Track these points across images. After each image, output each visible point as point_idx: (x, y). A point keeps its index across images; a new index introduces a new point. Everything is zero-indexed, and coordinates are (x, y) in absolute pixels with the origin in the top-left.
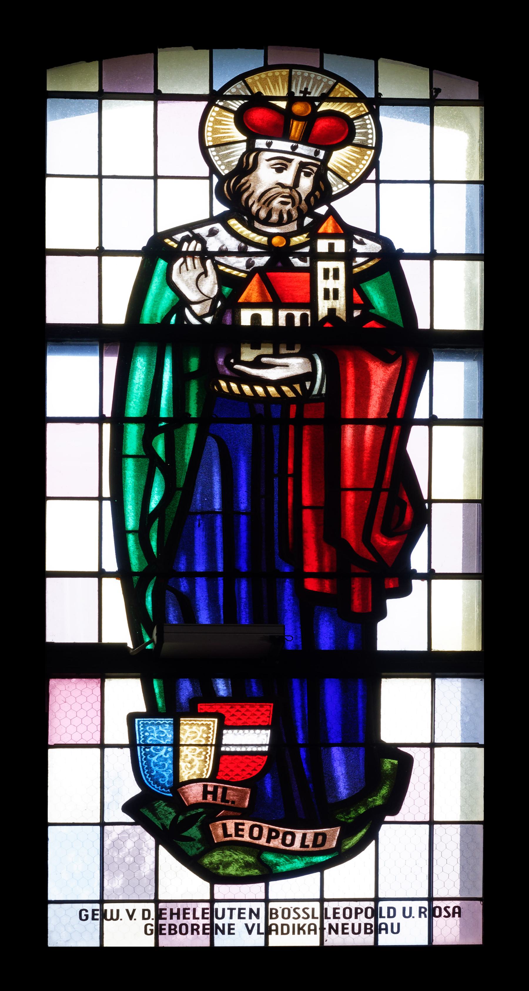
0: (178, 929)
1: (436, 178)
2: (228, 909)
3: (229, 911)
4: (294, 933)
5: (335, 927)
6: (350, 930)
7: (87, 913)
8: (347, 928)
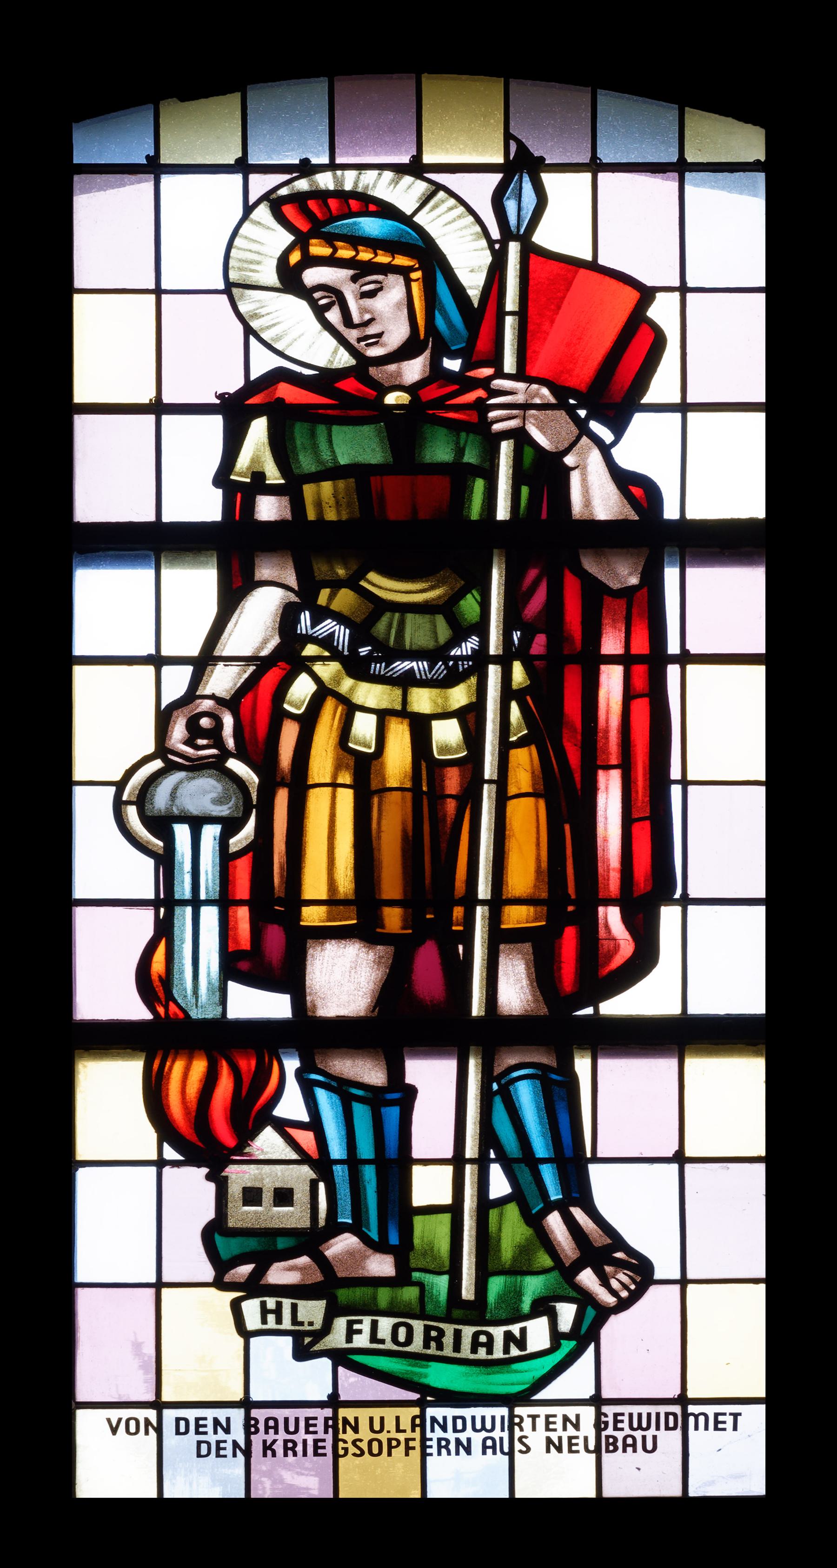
1: (164, 286)
2: (529, 1416)
3: (732, 1417)
4: (706, 1428)
6: (581, 1447)
7: (345, 1446)
8: (577, 1444)
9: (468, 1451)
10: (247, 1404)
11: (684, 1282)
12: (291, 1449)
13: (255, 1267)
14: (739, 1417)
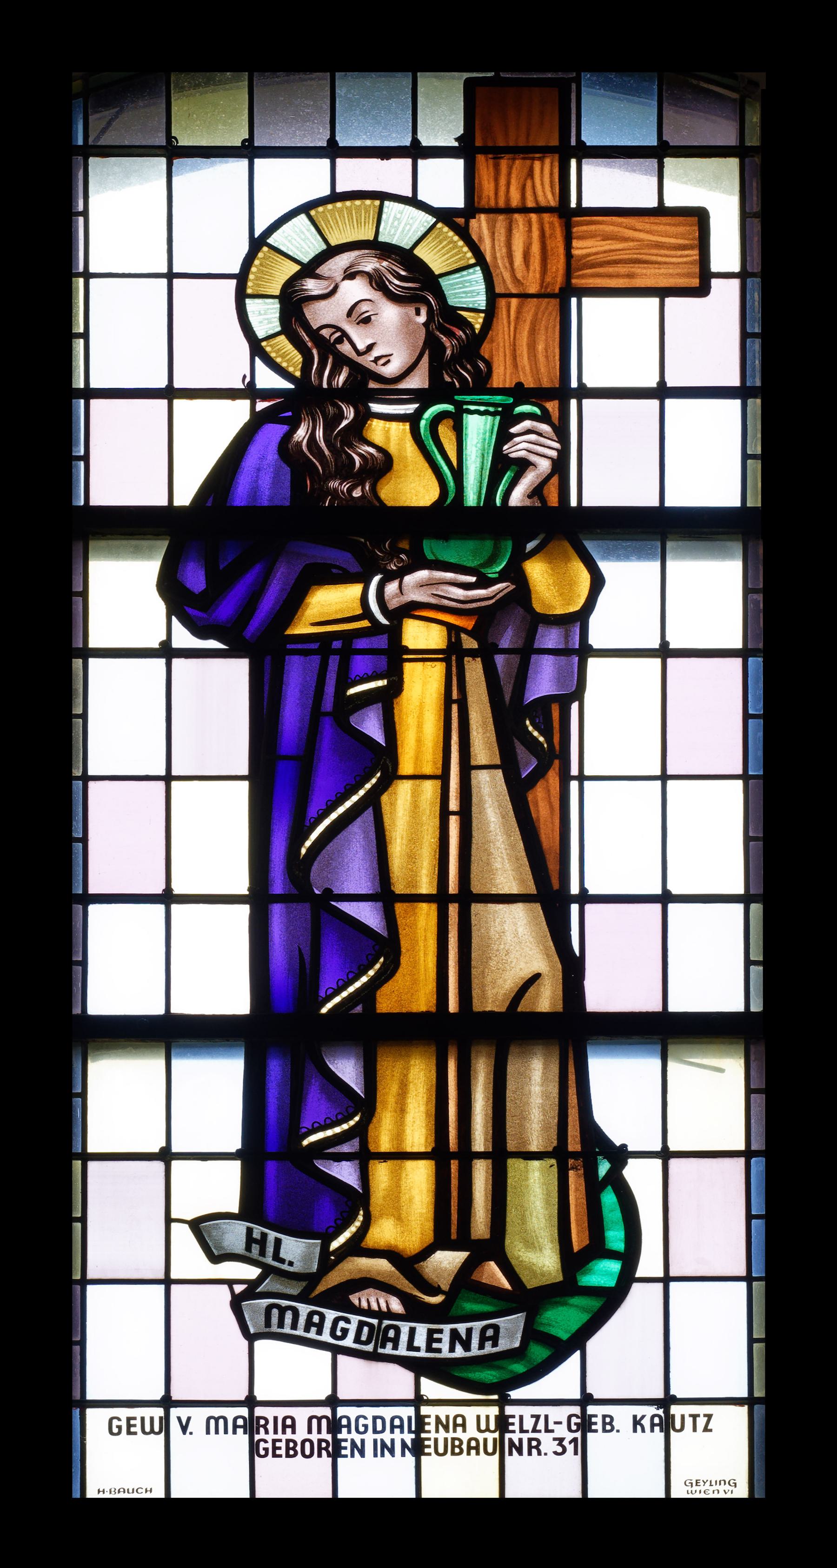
0: (298, 1448)
2: (690, 1416)
3: (691, 1419)
4: (226, 1432)
5: (517, 1443)
6: (138, 1429)
9: (362, 1453)
11: (666, 1280)
12: (535, 1447)
13: (469, 1256)
14: (698, 1419)
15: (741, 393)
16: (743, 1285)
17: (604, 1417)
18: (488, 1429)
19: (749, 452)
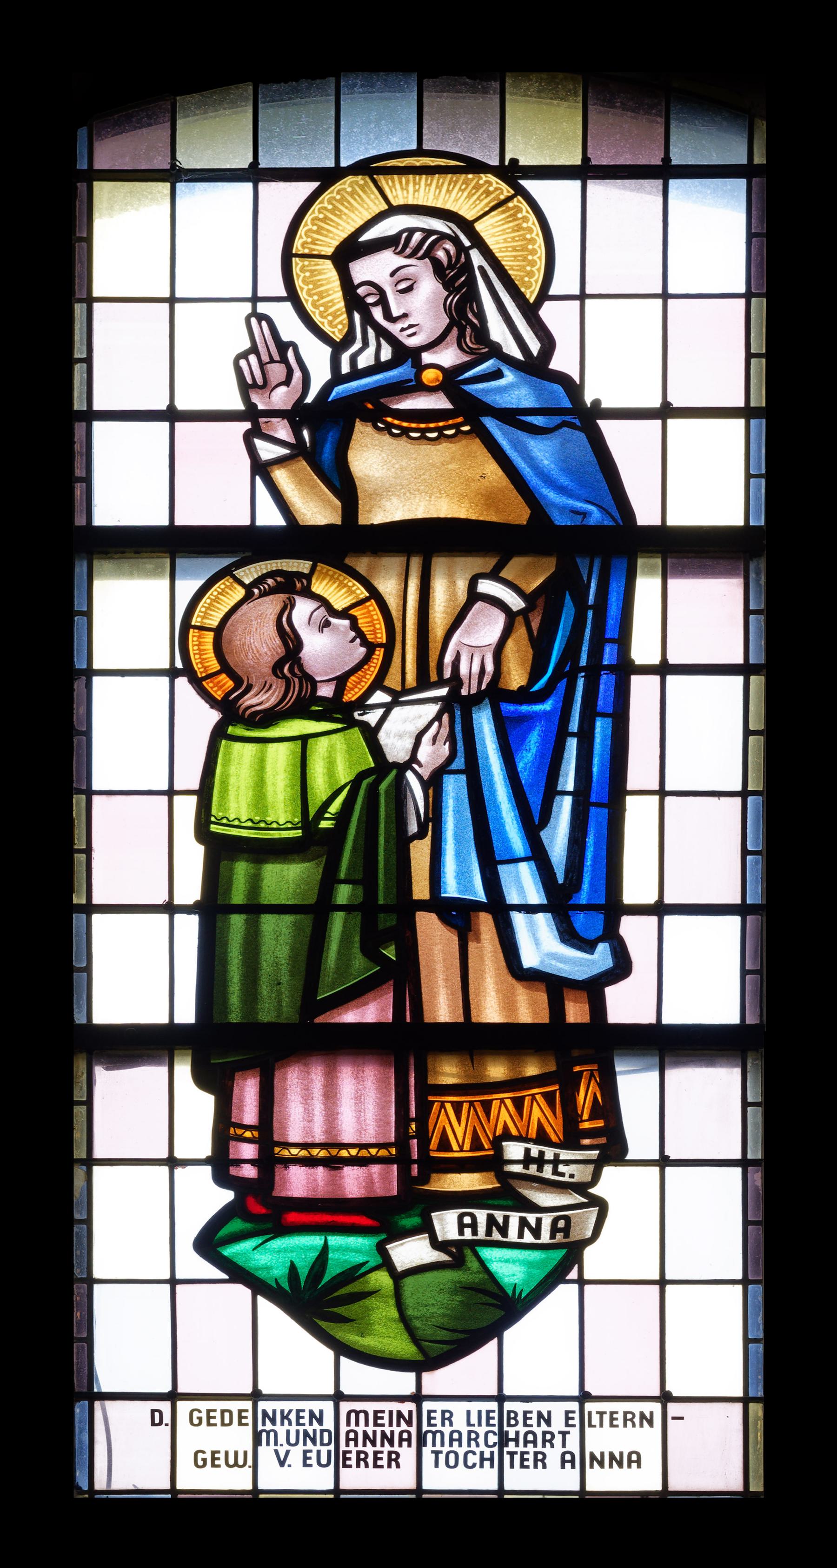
2: (598, 1413)
3: (598, 1416)
4: (236, 1453)
10: (338, 1397)
15: (744, 670)
16: (739, 1288)
17: (443, 1412)
18: (268, 1433)
19: (750, 1337)
